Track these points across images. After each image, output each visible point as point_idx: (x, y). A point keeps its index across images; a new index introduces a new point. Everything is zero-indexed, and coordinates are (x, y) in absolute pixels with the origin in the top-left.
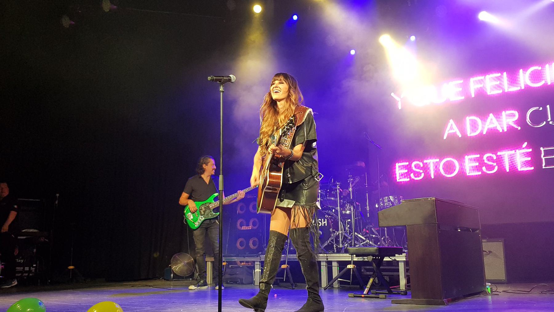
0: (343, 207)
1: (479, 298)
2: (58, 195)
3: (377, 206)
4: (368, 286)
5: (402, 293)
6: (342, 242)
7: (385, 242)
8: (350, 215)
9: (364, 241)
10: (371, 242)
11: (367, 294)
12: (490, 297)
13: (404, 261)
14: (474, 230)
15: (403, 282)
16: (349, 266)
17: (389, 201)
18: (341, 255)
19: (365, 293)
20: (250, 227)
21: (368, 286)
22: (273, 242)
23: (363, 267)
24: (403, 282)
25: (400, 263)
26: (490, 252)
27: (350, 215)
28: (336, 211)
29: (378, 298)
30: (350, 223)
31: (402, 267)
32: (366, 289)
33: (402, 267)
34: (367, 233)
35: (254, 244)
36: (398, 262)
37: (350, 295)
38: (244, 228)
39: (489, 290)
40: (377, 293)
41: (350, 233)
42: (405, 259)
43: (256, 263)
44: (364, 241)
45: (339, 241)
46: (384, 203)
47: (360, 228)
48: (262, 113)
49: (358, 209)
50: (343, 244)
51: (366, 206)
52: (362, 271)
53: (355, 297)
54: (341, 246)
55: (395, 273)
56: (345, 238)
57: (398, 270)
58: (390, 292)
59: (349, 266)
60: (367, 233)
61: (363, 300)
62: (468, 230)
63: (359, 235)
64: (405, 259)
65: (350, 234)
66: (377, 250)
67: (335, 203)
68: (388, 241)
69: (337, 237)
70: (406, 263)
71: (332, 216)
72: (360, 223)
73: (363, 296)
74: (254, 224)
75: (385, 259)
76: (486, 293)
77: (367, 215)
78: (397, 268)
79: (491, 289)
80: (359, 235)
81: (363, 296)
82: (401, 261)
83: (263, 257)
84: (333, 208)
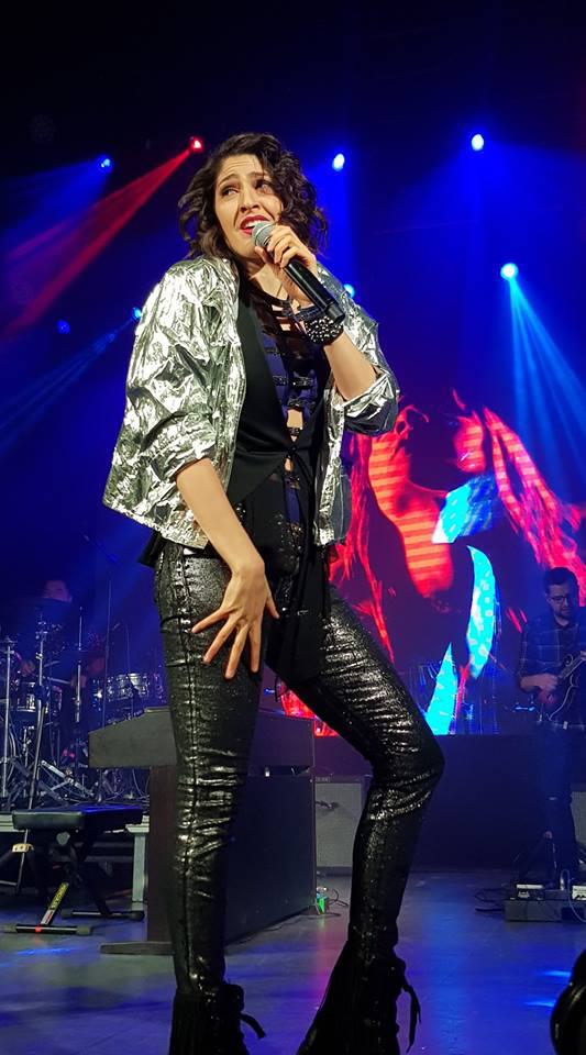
1: (295, 927)
2: (197, 145)
4: (54, 905)
5: (133, 915)
6: (8, 783)
8: (35, 714)
9: (61, 780)
11: (49, 925)
12: (322, 923)
13: (146, 834)
14: (299, 770)
17: (129, 685)
19: (43, 922)
21: (54, 905)
25: (136, 839)
26: (335, 805)
27: (35, 714)
29: (74, 933)
31: (140, 847)
32: (49, 912)
33: (140, 847)
36: (134, 835)
39: (322, 905)
42: (147, 830)
46: (116, 689)
48: (251, 215)
50: (9, 788)
51: (76, 696)
52: (51, 852)
53: (19, 931)
55: (125, 859)
57: (131, 852)
61: (37, 941)
62: (286, 770)
63: (51, 768)
66: (80, 818)
76: (314, 911)
77: (74, 717)
78: (125, 859)
79: (327, 900)
80: (51, 768)
81: (38, 929)
82: (140, 834)
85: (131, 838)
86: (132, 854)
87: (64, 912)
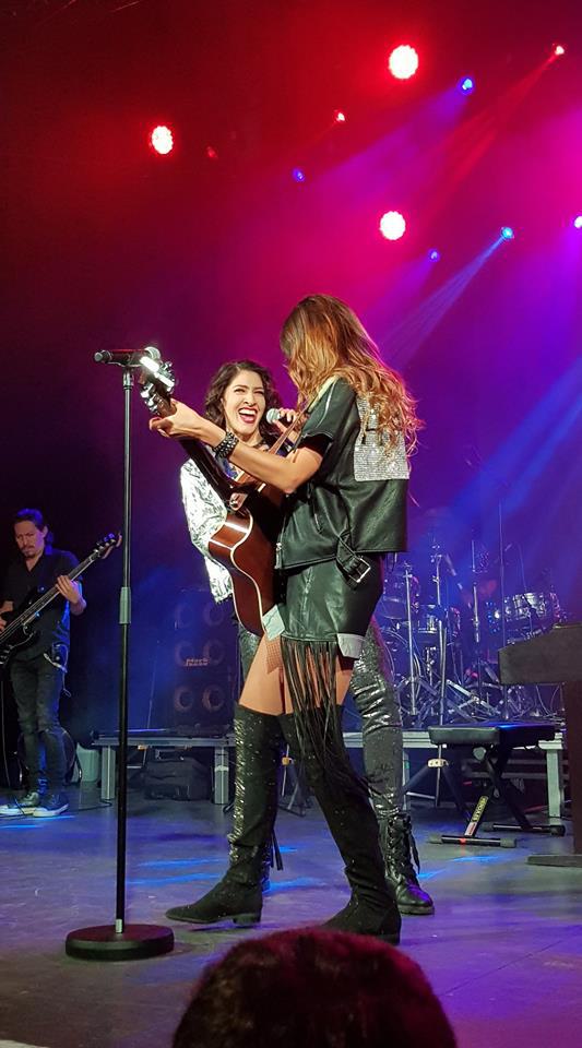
0: (419, 617)
3: (497, 616)
4: (476, 817)
5: (554, 830)
6: (417, 700)
7: (515, 699)
8: (436, 636)
9: (467, 698)
10: (483, 703)
11: (473, 836)
13: (558, 750)
15: (555, 798)
16: (433, 763)
17: (526, 605)
18: (415, 734)
19: (467, 834)
20: (205, 662)
21: (476, 817)
22: (280, 425)
23: (465, 761)
24: (555, 798)
27: (436, 636)
28: (404, 630)
29: (498, 845)
30: (435, 655)
31: (553, 763)
32: (471, 824)
33: (553, 763)
34: (474, 679)
35: (213, 701)
36: (545, 751)
37: (433, 840)
38: (190, 662)
40: (495, 830)
41: (436, 679)
42: (560, 747)
43: (217, 752)
44: (467, 698)
45: (410, 699)
47: (459, 673)
49: (453, 623)
50: (419, 706)
52: (463, 768)
53: (445, 842)
54: (414, 711)
56: (424, 694)
57: (544, 769)
58: (527, 828)
59: (433, 763)
60: (474, 679)
63: (456, 686)
64: (560, 747)
65: (434, 683)
67: (400, 610)
68: (522, 697)
69: (407, 689)
70: (563, 754)
71: (394, 640)
72: (457, 656)
73: (463, 840)
74: (213, 655)
75: (509, 762)
77: (474, 638)
80: (456, 686)
81: (463, 840)
82: (552, 751)
83: (254, 441)
84: (396, 621)
85: (543, 754)
86: (546, 772)
87: (484, 825)
